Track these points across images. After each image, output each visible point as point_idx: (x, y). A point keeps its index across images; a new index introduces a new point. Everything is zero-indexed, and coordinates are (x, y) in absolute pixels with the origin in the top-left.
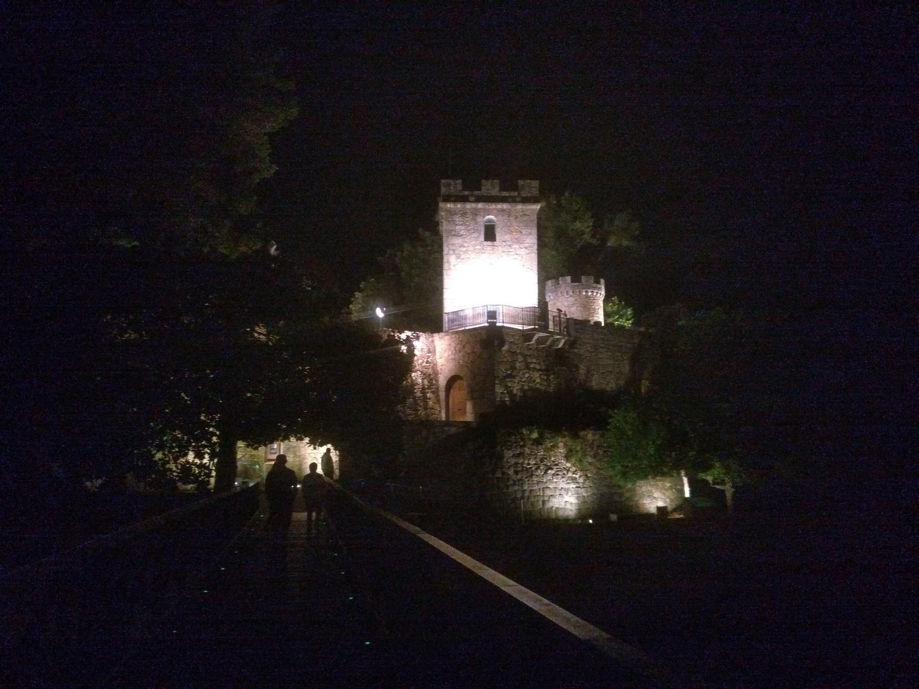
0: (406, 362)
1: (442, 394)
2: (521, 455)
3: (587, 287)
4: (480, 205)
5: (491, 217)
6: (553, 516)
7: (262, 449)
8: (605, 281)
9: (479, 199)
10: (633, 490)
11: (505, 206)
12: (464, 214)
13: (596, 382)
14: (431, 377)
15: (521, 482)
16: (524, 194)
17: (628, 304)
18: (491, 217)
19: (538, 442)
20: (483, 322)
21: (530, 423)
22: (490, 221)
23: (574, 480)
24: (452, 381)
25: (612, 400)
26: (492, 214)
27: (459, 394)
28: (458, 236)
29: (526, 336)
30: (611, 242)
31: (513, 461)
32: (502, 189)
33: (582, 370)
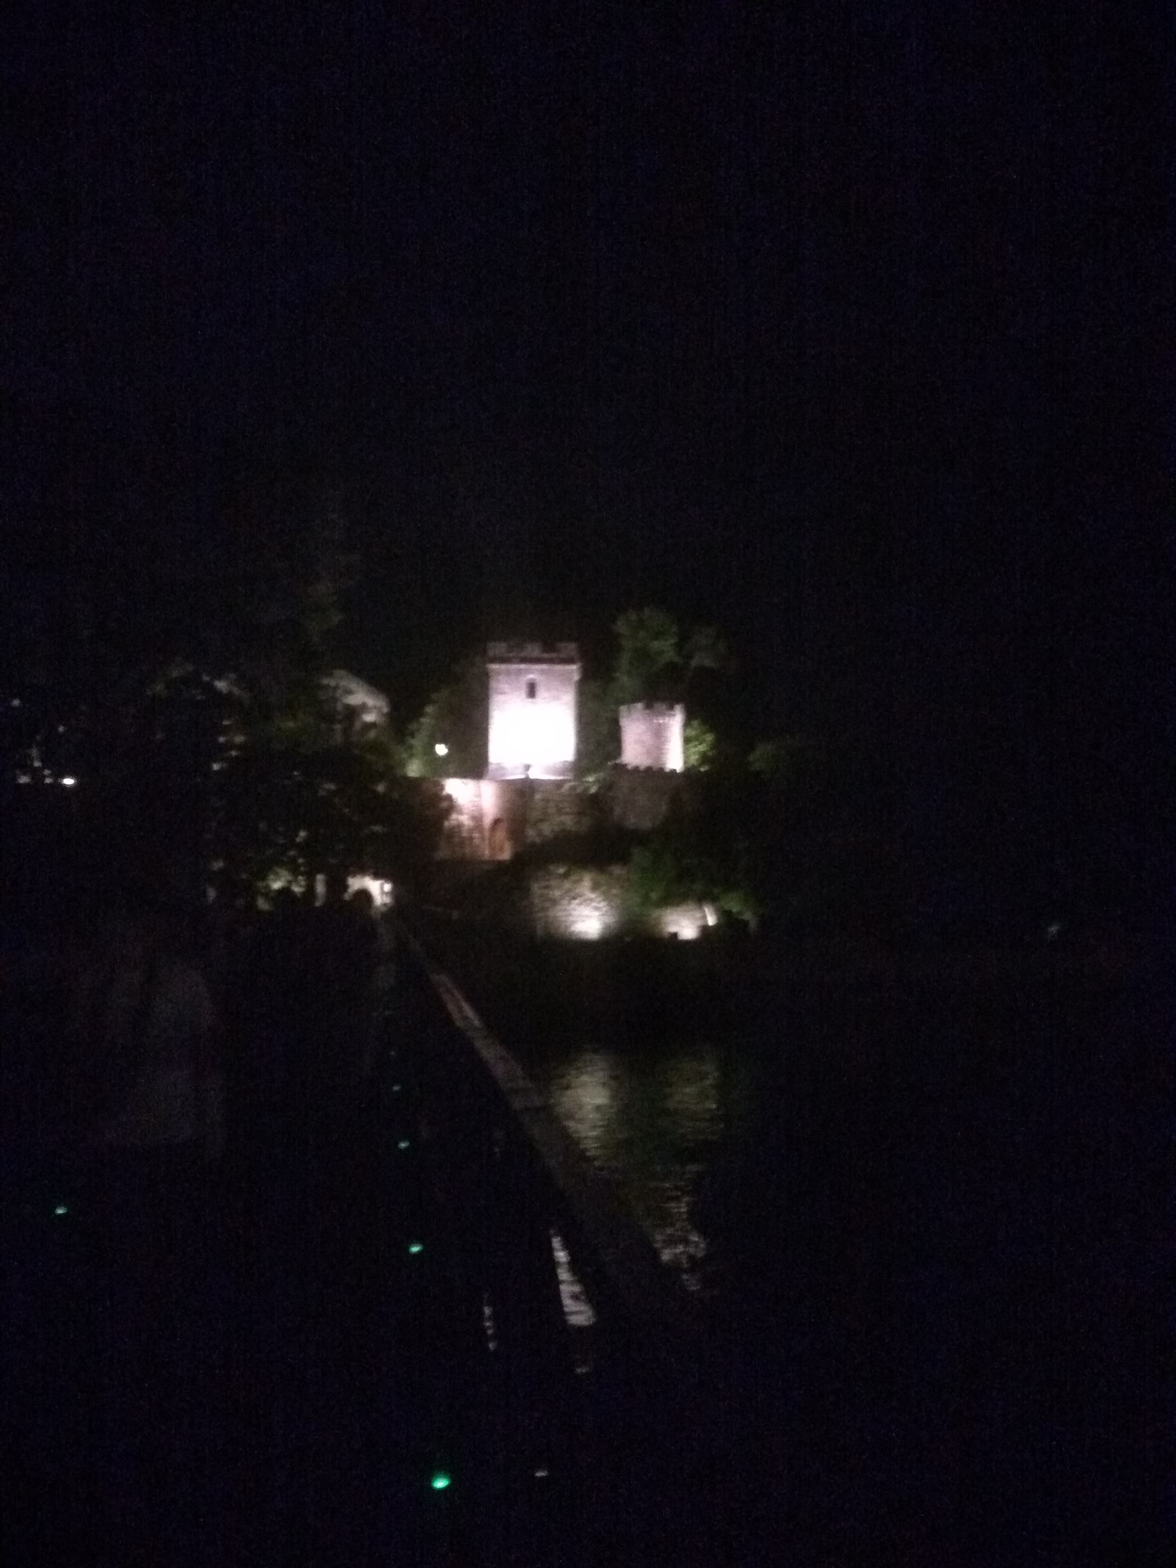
0: (450, 806)
1: (487, 834)
2: (547, 887)
3: (662, 714)
4: (523, 666)
5: (532, 676)
6: (574, 938)
7: (624, 643)
8: (354, 874)
9: (524, 660)
10: (659, 918)
11: (544, 667)
12: (508, 673)
13: (632, 822)
14: (478, 819)
15: (544, 909)
16: (562, 655)
17: (710, 731)
18: (532, 676)
19: (566, 876)
20: (519, 776)
21: (559, 859)
22: (532, 679)
23: (597, 909)
24: (497, 822)
25: (640, 838)
26: (534, 673)
27: (501, 834)
28: (503, 693)
29: (558, 785)
30: (694, 663)
31: (539, 892)
32: (545, 651)
33: (617, 811)
